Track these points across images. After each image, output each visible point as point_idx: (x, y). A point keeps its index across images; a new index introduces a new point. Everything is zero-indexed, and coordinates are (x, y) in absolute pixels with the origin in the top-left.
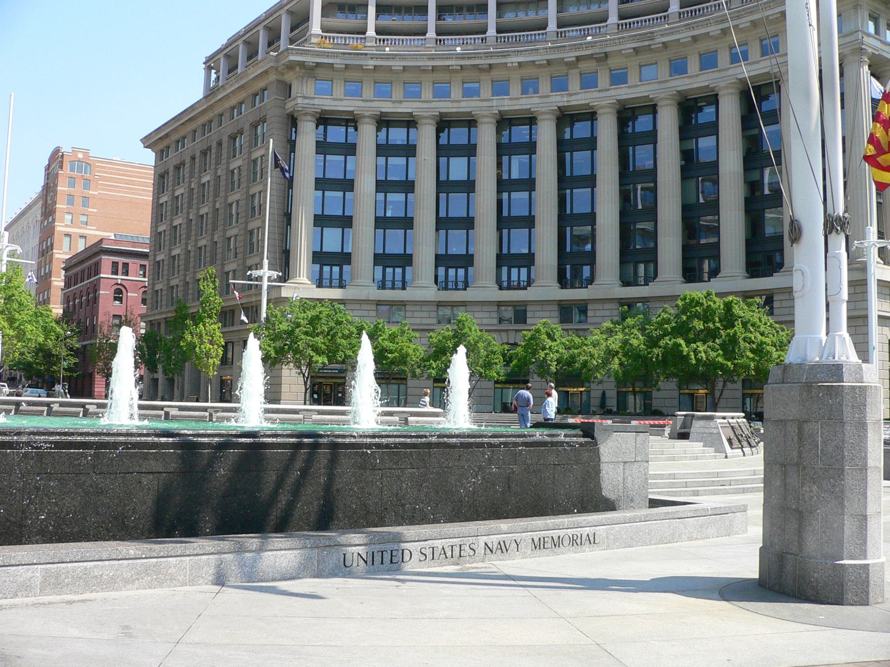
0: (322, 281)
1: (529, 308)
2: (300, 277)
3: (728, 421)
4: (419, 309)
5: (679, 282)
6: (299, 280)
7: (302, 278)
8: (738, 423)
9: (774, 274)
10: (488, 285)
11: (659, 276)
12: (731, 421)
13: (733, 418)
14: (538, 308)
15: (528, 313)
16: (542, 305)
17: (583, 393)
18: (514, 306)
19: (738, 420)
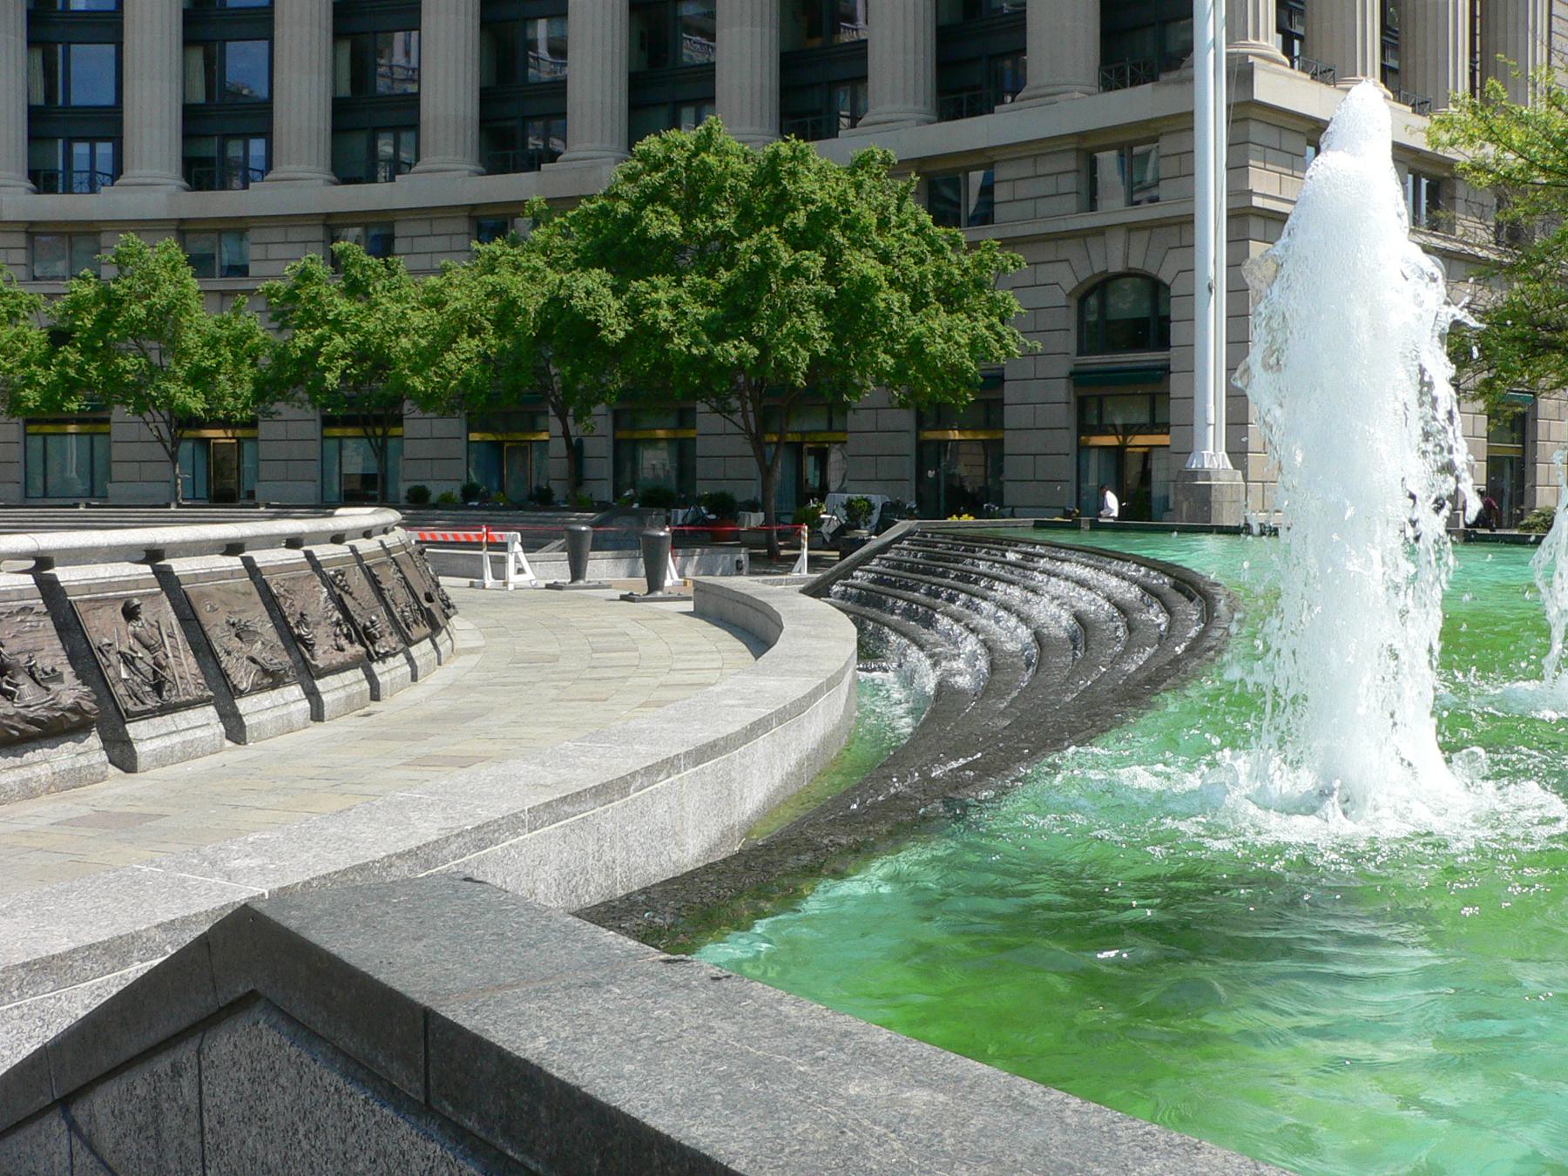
0: (71, 178)
1: (399, 230)
2: (1256, 37)
3: (353, 549)
4: (1029, 172)
5: (914, 122)
6: (1252, 46)
7: (1262, 42)
8: (388, 551)
9: (996, 108)
10: (300, 175)
11: (424, 159)
12: (323, 551)
13: (367, 534)
14: (423, 228)
15: (396, 241)
16: (431, 219)
17: (40, 493)
18: (366, 226)
19: (382, 537)
